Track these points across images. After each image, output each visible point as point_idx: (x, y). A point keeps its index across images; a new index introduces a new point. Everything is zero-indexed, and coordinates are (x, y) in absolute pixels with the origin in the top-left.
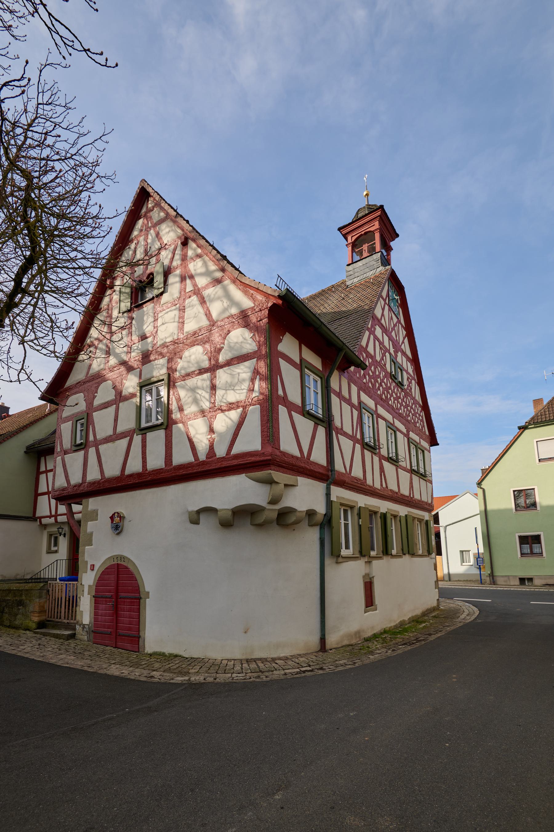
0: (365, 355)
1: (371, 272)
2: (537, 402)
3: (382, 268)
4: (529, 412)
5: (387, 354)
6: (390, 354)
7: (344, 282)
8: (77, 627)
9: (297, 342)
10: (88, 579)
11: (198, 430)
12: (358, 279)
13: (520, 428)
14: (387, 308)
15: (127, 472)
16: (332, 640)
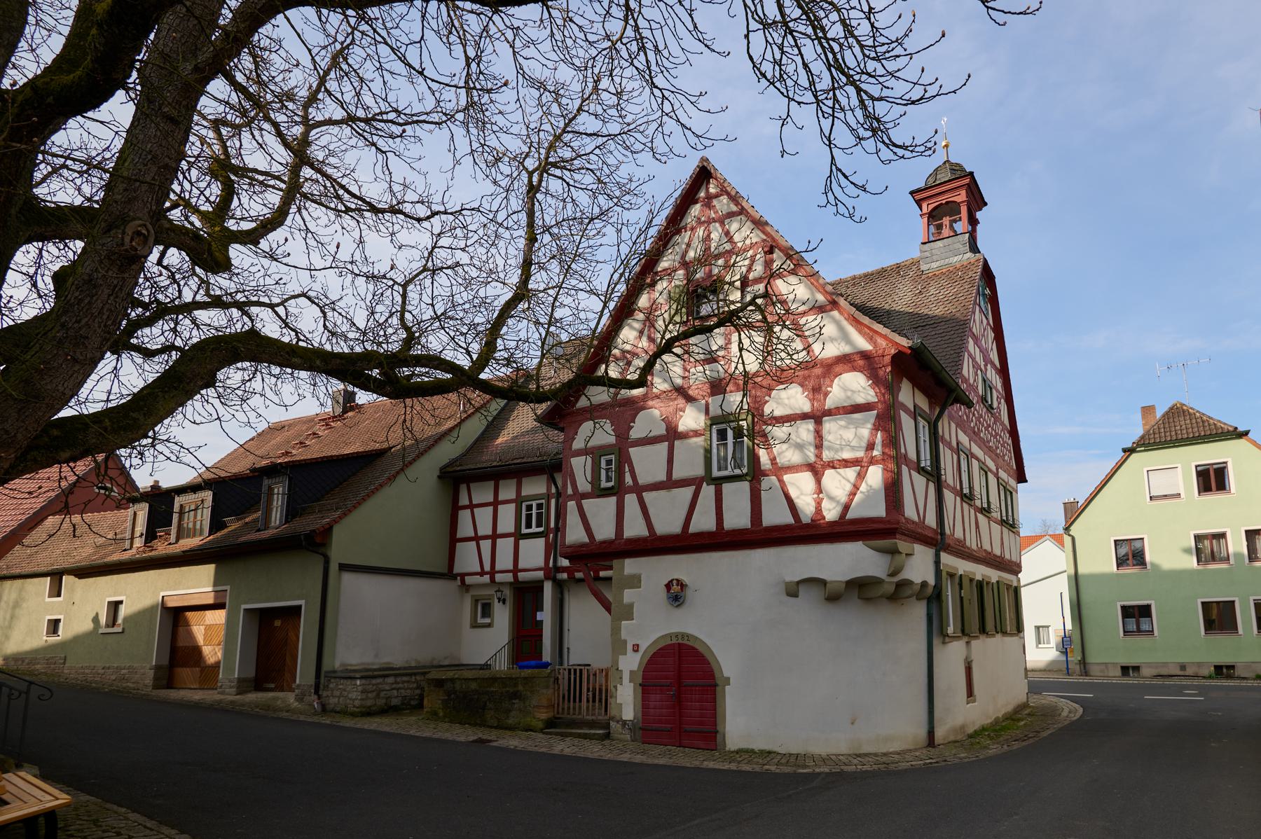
2: (1147, 411)
3: (969, 255)
4: (1136, 430)
7: (916, 263)
8: (612, 723)
9: (910, 385)
10: (630, 663)
11: (801, 487)
12: (938, 264)
13: (1125, 450)
15: (692, 529)
16: (940, 733)
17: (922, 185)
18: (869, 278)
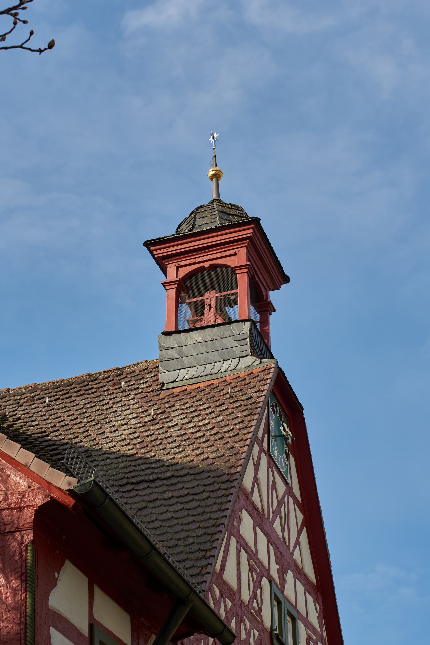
0: (217, 591)
1: (226, 365)
3: (250, 360)
5: (265, 582)
6: (271, 580)
7: (150, 369)
9: (84, 581)
14: (264, 460)
17: (170, 232)
18: (62, 390)
